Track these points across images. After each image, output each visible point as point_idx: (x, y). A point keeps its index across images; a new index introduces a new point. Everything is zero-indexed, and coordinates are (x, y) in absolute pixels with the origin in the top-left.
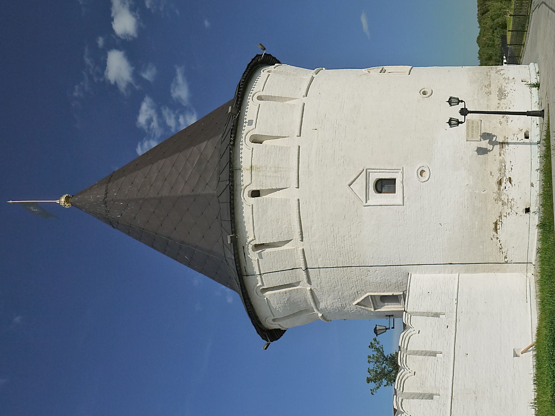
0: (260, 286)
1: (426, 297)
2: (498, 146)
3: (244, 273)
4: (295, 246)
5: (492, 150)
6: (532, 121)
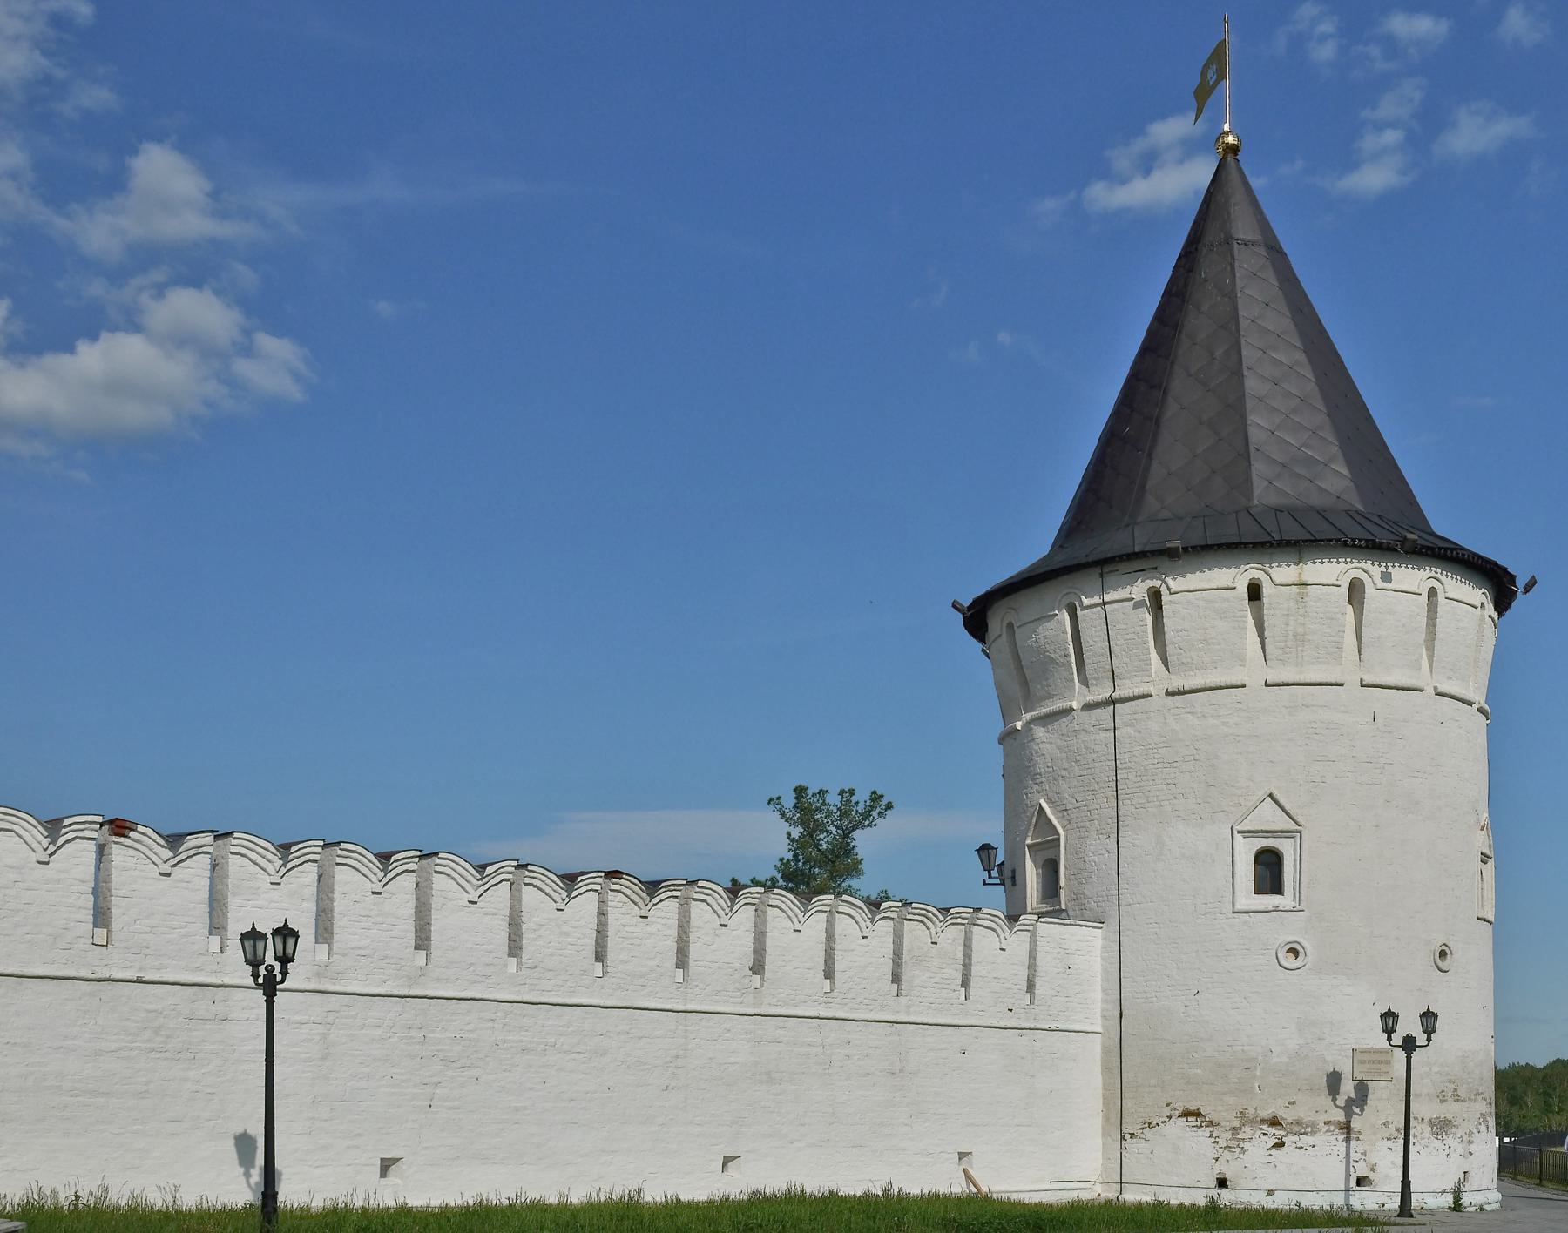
0: (1081, 601)
2: (1342, 1118)
4: (1157, 678)
5: (1335, 1104)
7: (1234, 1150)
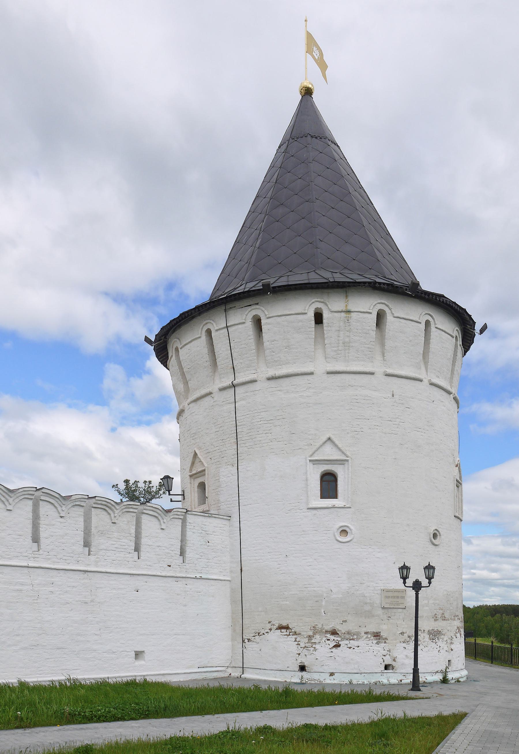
1: (203, 538)
3: (228, 306)
6: (405, 674)
7: (309, 649)
